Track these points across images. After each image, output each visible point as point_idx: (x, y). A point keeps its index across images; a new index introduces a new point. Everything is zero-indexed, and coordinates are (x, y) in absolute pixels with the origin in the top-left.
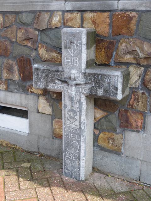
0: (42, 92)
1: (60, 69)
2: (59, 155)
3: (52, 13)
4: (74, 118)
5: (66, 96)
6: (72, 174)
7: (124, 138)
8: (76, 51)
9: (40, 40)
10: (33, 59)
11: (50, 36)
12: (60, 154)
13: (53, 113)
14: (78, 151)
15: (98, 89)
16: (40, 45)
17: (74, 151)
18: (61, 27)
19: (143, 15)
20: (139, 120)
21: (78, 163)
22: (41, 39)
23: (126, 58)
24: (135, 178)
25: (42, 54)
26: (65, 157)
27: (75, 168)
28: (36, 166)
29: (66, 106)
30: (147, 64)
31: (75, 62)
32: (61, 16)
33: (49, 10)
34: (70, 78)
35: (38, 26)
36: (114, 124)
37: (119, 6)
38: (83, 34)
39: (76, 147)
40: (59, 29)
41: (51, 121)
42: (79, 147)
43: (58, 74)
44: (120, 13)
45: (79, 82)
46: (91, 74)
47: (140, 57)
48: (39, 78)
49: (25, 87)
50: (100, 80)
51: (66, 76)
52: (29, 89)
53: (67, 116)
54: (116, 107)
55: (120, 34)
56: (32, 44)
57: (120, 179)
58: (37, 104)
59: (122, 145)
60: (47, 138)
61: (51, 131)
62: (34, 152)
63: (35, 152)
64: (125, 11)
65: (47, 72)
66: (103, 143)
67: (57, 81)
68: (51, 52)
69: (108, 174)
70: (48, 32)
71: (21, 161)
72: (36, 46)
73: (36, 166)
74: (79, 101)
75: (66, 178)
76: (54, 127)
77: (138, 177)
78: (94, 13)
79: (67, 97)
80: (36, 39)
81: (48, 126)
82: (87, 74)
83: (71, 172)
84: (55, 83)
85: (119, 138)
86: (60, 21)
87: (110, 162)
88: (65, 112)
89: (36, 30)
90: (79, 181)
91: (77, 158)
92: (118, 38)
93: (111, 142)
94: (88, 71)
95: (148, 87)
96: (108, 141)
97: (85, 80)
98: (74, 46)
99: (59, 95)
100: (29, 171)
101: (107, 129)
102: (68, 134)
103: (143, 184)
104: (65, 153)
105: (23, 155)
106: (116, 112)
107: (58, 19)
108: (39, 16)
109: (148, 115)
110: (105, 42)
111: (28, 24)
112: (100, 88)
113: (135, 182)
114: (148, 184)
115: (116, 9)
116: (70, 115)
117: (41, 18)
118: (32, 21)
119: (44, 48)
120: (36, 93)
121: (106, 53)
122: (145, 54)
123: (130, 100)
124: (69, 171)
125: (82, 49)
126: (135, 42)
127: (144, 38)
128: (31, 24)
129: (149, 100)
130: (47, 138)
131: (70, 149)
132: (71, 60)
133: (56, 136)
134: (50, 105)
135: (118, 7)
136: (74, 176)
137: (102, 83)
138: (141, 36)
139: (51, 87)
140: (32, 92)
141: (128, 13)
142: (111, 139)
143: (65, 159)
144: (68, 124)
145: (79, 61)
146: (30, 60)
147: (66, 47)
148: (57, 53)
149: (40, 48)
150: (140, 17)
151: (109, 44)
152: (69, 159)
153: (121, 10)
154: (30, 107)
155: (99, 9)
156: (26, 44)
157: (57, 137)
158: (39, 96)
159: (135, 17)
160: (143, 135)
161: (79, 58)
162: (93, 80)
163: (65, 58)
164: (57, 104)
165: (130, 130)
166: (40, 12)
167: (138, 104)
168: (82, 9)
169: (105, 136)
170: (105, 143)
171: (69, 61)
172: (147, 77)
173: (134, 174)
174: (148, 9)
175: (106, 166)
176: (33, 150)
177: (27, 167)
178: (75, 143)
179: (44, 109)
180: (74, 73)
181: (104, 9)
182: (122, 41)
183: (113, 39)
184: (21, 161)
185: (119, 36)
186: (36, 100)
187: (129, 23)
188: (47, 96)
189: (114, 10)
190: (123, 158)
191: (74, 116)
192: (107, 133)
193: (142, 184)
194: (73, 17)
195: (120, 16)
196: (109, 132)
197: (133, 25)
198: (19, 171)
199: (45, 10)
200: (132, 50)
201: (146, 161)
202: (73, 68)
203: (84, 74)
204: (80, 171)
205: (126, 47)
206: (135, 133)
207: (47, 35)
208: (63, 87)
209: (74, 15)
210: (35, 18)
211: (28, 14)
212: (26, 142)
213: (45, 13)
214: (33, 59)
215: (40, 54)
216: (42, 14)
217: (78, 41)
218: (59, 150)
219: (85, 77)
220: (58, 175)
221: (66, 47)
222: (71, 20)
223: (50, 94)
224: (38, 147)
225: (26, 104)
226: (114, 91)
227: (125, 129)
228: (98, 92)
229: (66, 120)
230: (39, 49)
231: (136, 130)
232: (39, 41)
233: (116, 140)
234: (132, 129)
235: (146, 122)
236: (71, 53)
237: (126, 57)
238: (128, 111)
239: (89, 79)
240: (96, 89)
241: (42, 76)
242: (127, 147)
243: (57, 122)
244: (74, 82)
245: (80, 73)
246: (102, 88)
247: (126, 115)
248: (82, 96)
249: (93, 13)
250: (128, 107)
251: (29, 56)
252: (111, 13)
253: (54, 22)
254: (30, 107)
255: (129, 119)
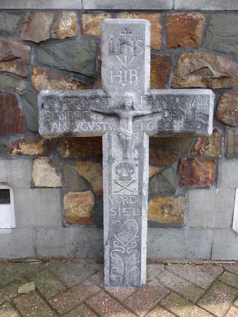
0: (42, 150)
1: (100, 93)
2: (77, 253)
3: (57, 14)
4: (129, 178)
5: (113, 140)
6: (124, 279)
7: (188, 202)
8: (133, 59)
9: (34, 60)
10: (21, 96)
11: (56, 52)
12: (77, 251)
13: (64, 183)
14: (137, 235)
15: (175, 121)
16: (36, 70)
17: (128, 237)
18: (76, 36)
19: (213, 16)
20: (210, 171)
21: (136, 257)
22: (36, 60)
23: (189, 81)
24: (204, 257)
25: (41, 85)
26: (110, 253)
27: (130, 266)
28: (48, 283)
29: (111, 159)
30: (222, 87)
31: (131, 78)
32: (76, 20)
33: (50, 9)
34: (123, 107)
35: (31, 36)
36: (172, 183)
37: (176, 4)
38: (146, 28)
39: (133, 230)
40: (73, 40)
41: (59, 197)
42: (138, 228)
43: (97, 101)
44: (178, 14)
45: (140, 112)
46: (162, 96)
47: (214, 77)
48: (55, 114)
49: (5, 146)
50: (178, 106)
51: (113, 105)
52: (13, 149)
53: (114, 176)
54: (174, 156)
55: (179, 46)
56: (17, 68)
57: (184, 264)
58: (31, 173)
59: (184, 212)
60: (52, 228)
61: (60, 214)
62: (25, 259)
63: (29, 258)
64: (185, 11)
65: (73, 101)
66: (153, 216)
67: (94, 116)
68: (59, 79)
69: (165, 262)
70: (51, 47)
71: (11, 283)
72: (27, 72)
73: (48, 283)
74: (139, 147)
75: (116, 290)
76: (66, 207)
77: (209, 254)
78: (134, 15)
79: (115, 142)
80: (28, 58)
81: (54, 208)
82: (154, 98)
83: (123, 276)
84: (90, 120)
85: (179, 202)
86: (73, 28)
87: (171, 243)
88: (110, 169)
89: (26, 44)
90: (138, 288)
91: (134, 249)
92: (176, 51)
93: (166, 211)
94: (156, 92)
95: (223, 120)
96: (161, 211)
97: (150, 107)
98: (128, 49)
99: (96, 142)
100: (39, 300)
101: (160, 193)
102: (116, 210)
103: (218, 262)
104: (112, 245)
105: (10, 270)
106: (173, 165)
107: (70, 24)
108: (30, 19)
109: (222, 161)
110: (156, 58)
111: (8, 33)
112: (178, 120)
113: (204, 262)
114: (224, 261)
115: (171, 9)
116: (120, 175)
117: (35, 22)
118: (17, 28)
119: (44, 74)
120: (28, 155)
121: (159, 75)
122: (221, 72)
123: (195, 143)
124: (119, 274)
125: (144, 53)
126: (203, 56)
127: (215, 50)
128: (15, 33)
129: (224, 139)
130: (52, 228)
131: (121, 235)
132: (123, 74)
133: (70, 222)
134: (57, 172)
135: (174, 5)
136: (129, 282)
137: (182, 110)
138: (211, 48)
139: (81, 128)
140: (20, 154)
141: (189, 15)
142: (166, 206)
143: (110, 257)
144: (117, 192)
145: (138, 75)
146: (14, 97)
147: (112, 52)
148: (69, 82)
149: (36, 75)
150: (208, 20)
151: (163, 61)
152: (119, 253)
153: (179, 11)
154: (17, 181)
155: (143, 8)
156: (4, 69)
157: (72, 222)
158: (34, 158)
159: (202, 19)
160: (214, 191)
161: (139, 71)
162: (165, 106)
163: (111, 71)
164: (72, 167)
165: (195, 188)
166: (33, 11)
167: (207, 147)
168: (113, 9)
169: (157, 203)
170: (157, 214)
171: (119, 78)
172: (222, 105)
173: (203, 251)
174: (219, 9)
175: (159, 250)
176: (24, 255)
177: (31, 293)
178: (130, 222)
179: (45, 180)
180: (131, 96)
181: (152, 9)
182: (183, 56)
183: (170, 53)
184: (11, 283)
185: (178, 49)
186: (29, 167)
187: (194, 29)
188: (52, 156)
189: (167, 11)
190: (186, 232)
191: (129, 174)
192: (160, 199)
193: (216, 262)
194: (98, 22)
195: (177, 19)
196: (163, 197)
197: (199, 32)
198: (19, 306)
199: (44, 8)
200: (201, 67)
201: (220, 228)
202: (127, 89)
203: (150, 98)
204: (140, 270)
205: (191, 63)
206: (204, 190)
207: (48, 52)
208: (106, 124)
209: (100, 17)
210: (21, 22)
211: (7, 15)
212: (10, 245)
213: (43, 13)
214: (21, 96)
215: (36, 85)
216: (36, 16)
217: (137, 39)
218: (77, 243)
219: (149, 104)
220: (97, 289)
221: (112, 52)
222: (95, 26)
223: (58, 152)
224: (34, 247)
225: (7, 178)
226: (203, 121)
227: (188, 188)
228: (175, 127)
229: (114, 186)
230: (33, 77)
231: (203, 186)
232: (32, 62)
233: (175, 207)
234: (199, 186)
235: (219, 171)
236: (123, 61)
237: (190, 79)
238: (194, 159)
239: (158, 105)
240: (170, 121)
241: (60, 109)
242: (192, 213)
243: (71, 197)
244: (132, 113)
245: (141, 97)
246: (181, 118)
247: (191, 166)
248: (145, 138)
249: (133, 15)
250: (192, 153)
251: (12, 90)
252: (164, 15)
253: (63, 29)
254: (17, 181)
255: (196, 172)
